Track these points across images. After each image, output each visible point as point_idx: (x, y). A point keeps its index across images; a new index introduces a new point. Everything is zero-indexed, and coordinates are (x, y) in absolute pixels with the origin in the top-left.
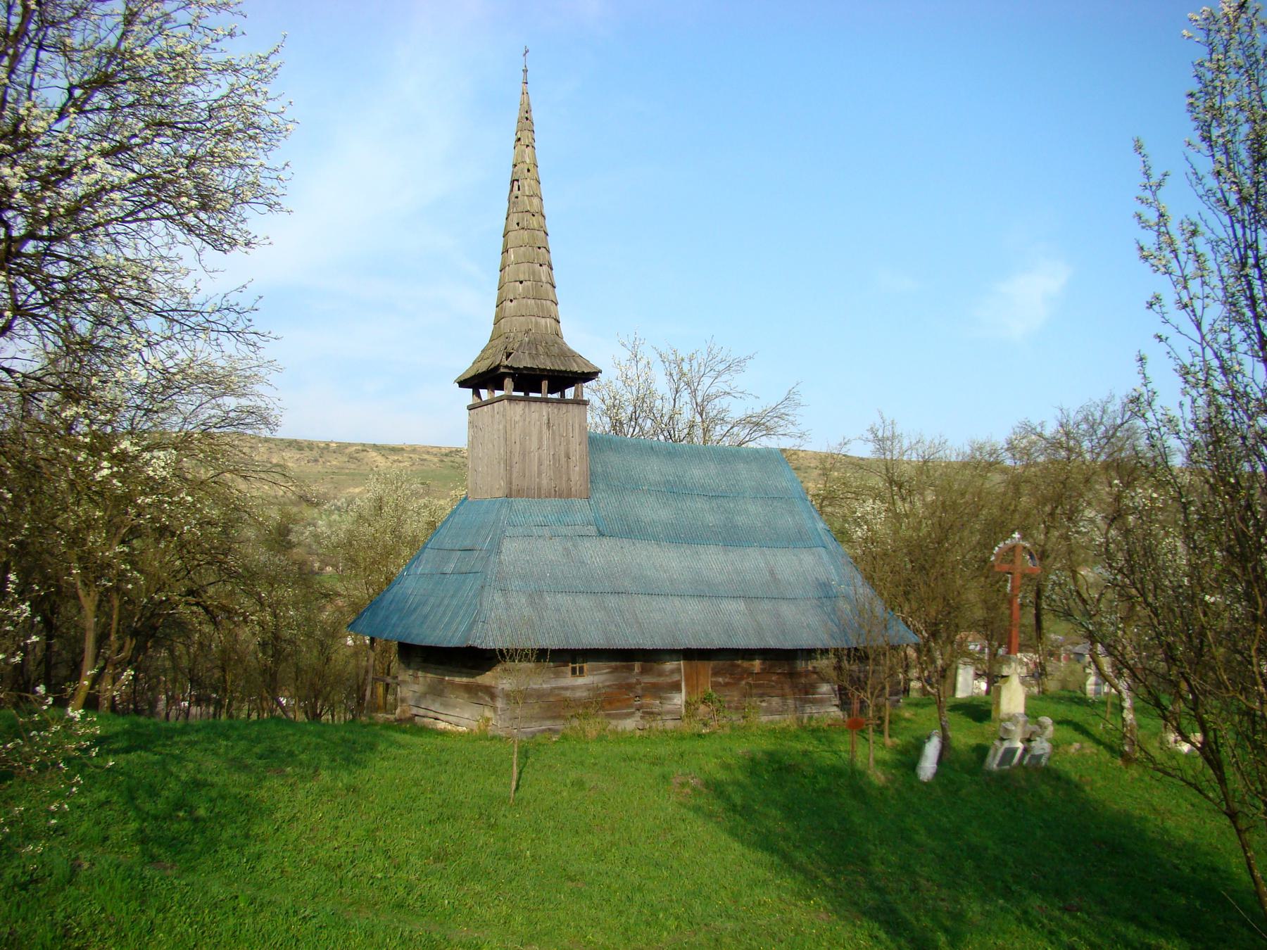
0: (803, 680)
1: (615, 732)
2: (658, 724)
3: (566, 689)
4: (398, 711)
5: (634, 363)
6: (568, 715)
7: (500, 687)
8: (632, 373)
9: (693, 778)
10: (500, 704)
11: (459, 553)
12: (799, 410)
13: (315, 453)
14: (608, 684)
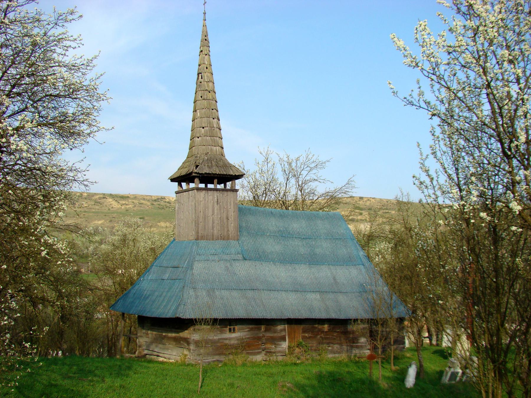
0: (351, 336)
1: (252, 362)
3: (226, 339)
4: (137, 353)
5: (266, 163)
6: (227, 353)
7: (192, 338)
8: (265, 169)
9: (288, 383)
10: (192, 347)
11: (171, 269)
14: (248, 337)
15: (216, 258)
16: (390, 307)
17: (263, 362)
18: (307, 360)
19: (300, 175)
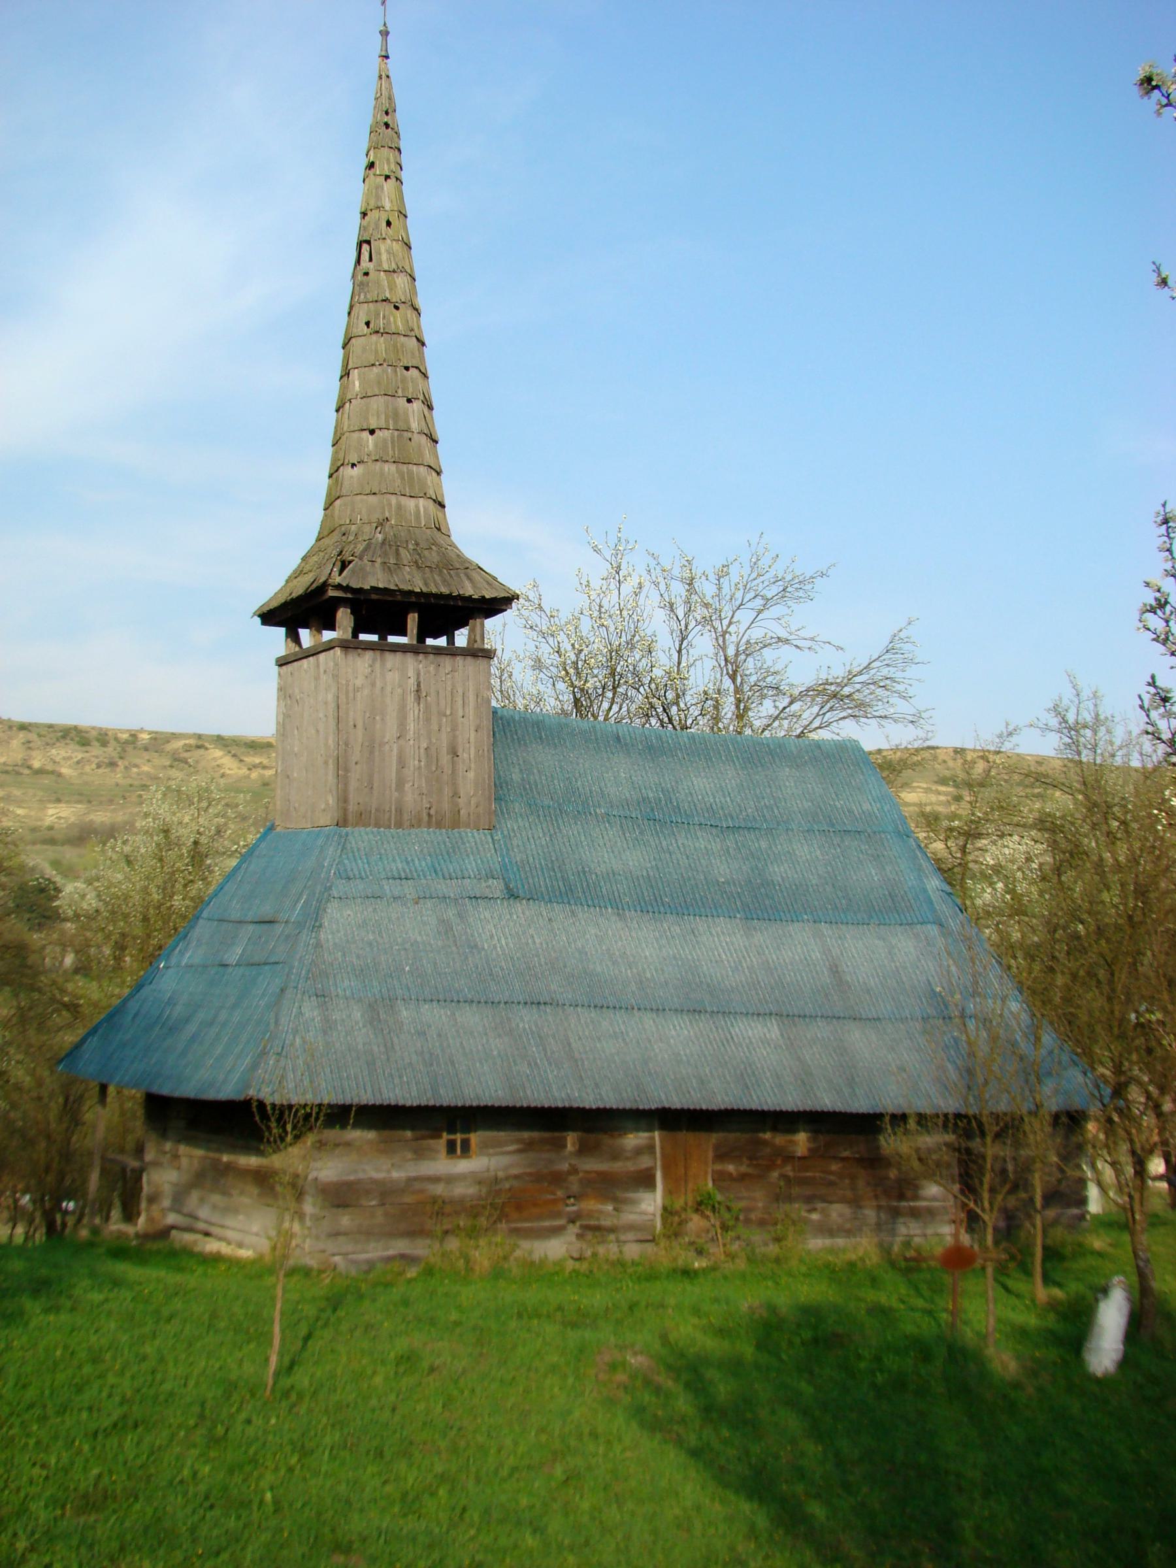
2: (609, 1249)
3: (436, 1179)
5: (613, 584)
8: (610, 601)
10: (309, 1207)
11: (251, 927)
12: (912, 671)
13: (111, 751)
15: (408, 889)
16: (1033, 1074)
17: (570, 1265)
18: (731, 1256)
19: (730, 623)
